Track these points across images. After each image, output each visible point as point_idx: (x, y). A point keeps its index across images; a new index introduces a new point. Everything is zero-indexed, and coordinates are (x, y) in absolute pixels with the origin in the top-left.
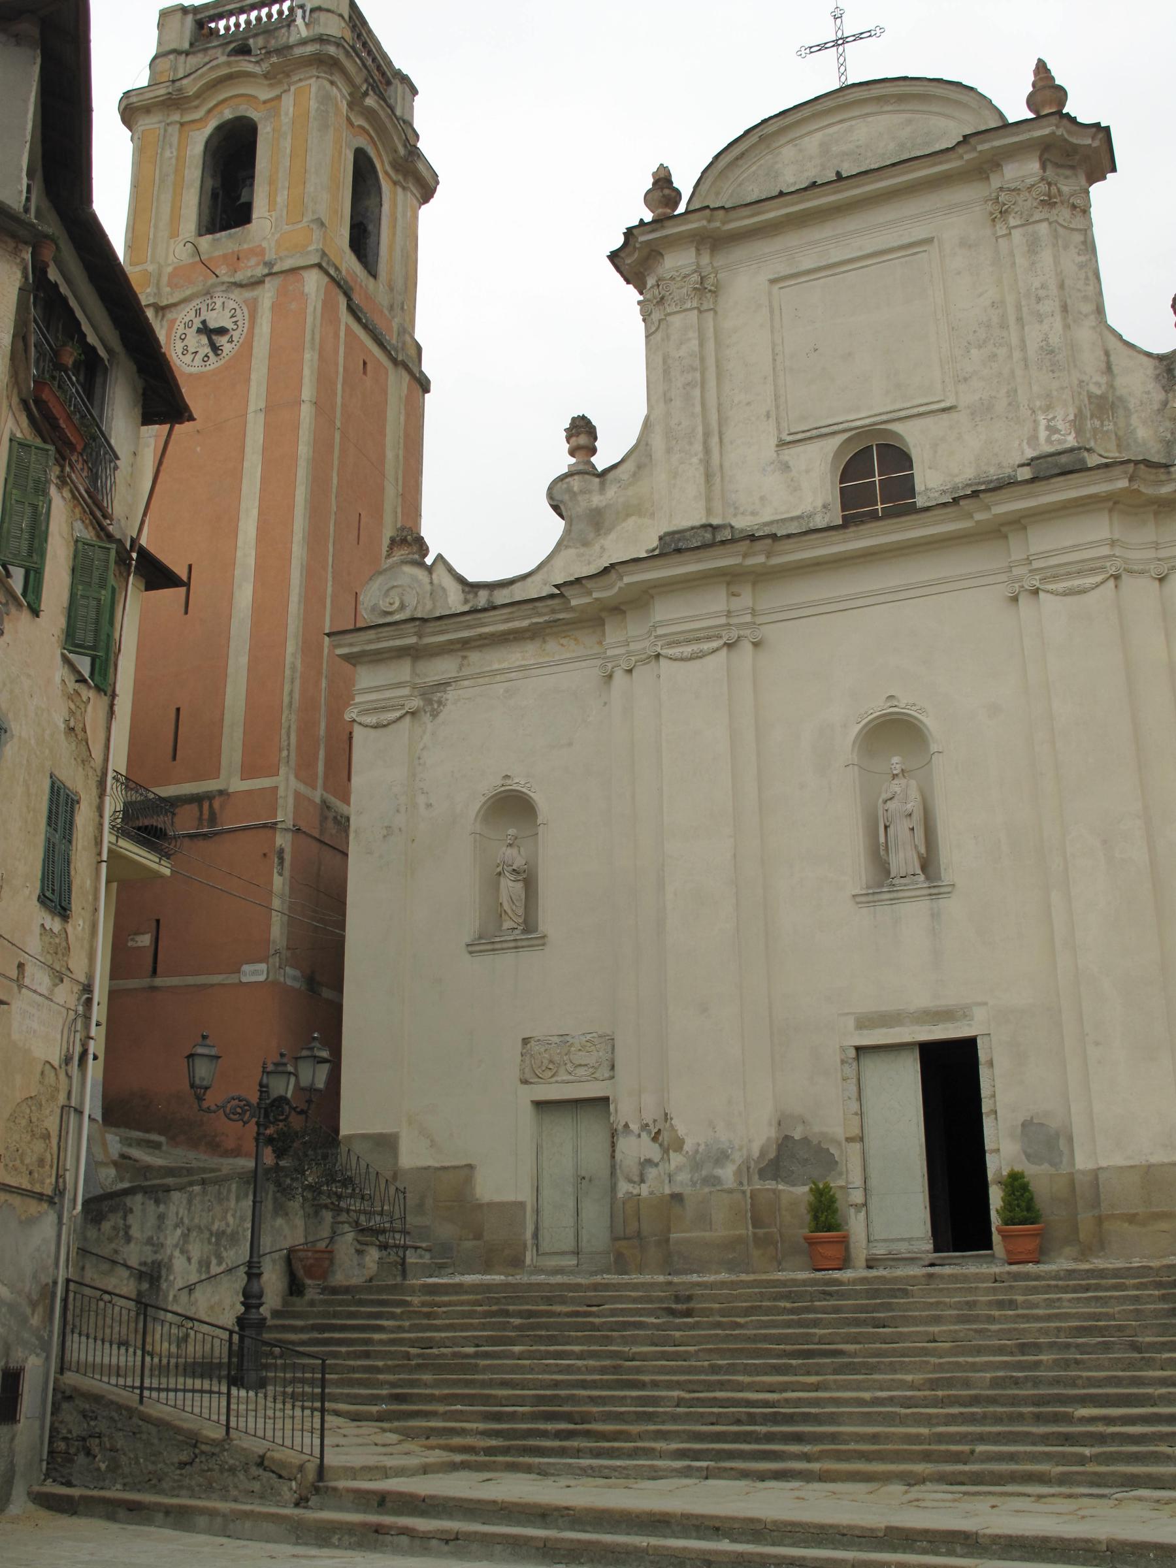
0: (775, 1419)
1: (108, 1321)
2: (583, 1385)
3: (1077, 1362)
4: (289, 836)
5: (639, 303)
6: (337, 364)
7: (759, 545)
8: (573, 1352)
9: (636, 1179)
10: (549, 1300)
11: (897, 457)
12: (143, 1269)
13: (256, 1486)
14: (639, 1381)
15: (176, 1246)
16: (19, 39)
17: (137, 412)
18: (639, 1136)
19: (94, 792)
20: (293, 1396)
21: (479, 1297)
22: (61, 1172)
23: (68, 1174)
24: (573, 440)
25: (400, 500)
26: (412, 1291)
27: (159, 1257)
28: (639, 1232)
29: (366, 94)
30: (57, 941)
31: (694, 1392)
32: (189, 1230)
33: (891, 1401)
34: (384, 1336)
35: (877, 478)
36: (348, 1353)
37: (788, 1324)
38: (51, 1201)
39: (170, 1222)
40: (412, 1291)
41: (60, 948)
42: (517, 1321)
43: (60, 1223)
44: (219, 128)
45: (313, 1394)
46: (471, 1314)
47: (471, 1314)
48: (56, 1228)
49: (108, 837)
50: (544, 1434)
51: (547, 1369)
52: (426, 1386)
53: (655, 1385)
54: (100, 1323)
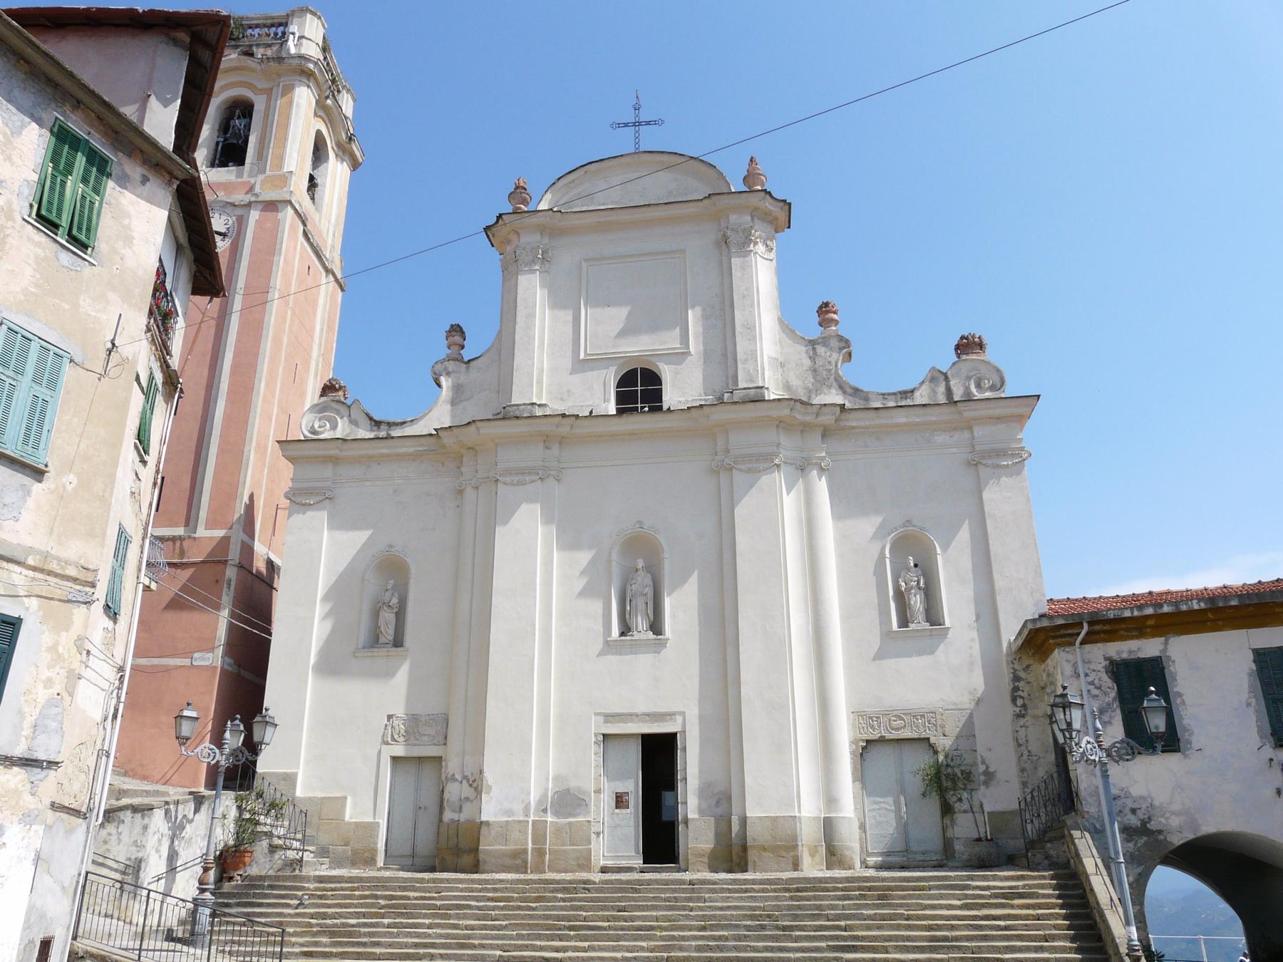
1: (98, 900)
2: (433, 946)
3: (746, 936)
4: (235, 569)
7: (566, 421)
16: (176, 42)
17: (189, 287)
20: (230, 953)
24: (451, 339)
27: (140, 855)
29: (327, 97)
37: (562, 909)
39: (151, 831)
40: (307, 879)
41: (110, 641)
42: (382, 902)
43: (88, 832)
44: (227, 100)
45: (274, 953)
46: (350, 897)
47: (350, 897)
51: (409, 935)
52: (325, 946)
53: (483, 946)
54: (92, 901)
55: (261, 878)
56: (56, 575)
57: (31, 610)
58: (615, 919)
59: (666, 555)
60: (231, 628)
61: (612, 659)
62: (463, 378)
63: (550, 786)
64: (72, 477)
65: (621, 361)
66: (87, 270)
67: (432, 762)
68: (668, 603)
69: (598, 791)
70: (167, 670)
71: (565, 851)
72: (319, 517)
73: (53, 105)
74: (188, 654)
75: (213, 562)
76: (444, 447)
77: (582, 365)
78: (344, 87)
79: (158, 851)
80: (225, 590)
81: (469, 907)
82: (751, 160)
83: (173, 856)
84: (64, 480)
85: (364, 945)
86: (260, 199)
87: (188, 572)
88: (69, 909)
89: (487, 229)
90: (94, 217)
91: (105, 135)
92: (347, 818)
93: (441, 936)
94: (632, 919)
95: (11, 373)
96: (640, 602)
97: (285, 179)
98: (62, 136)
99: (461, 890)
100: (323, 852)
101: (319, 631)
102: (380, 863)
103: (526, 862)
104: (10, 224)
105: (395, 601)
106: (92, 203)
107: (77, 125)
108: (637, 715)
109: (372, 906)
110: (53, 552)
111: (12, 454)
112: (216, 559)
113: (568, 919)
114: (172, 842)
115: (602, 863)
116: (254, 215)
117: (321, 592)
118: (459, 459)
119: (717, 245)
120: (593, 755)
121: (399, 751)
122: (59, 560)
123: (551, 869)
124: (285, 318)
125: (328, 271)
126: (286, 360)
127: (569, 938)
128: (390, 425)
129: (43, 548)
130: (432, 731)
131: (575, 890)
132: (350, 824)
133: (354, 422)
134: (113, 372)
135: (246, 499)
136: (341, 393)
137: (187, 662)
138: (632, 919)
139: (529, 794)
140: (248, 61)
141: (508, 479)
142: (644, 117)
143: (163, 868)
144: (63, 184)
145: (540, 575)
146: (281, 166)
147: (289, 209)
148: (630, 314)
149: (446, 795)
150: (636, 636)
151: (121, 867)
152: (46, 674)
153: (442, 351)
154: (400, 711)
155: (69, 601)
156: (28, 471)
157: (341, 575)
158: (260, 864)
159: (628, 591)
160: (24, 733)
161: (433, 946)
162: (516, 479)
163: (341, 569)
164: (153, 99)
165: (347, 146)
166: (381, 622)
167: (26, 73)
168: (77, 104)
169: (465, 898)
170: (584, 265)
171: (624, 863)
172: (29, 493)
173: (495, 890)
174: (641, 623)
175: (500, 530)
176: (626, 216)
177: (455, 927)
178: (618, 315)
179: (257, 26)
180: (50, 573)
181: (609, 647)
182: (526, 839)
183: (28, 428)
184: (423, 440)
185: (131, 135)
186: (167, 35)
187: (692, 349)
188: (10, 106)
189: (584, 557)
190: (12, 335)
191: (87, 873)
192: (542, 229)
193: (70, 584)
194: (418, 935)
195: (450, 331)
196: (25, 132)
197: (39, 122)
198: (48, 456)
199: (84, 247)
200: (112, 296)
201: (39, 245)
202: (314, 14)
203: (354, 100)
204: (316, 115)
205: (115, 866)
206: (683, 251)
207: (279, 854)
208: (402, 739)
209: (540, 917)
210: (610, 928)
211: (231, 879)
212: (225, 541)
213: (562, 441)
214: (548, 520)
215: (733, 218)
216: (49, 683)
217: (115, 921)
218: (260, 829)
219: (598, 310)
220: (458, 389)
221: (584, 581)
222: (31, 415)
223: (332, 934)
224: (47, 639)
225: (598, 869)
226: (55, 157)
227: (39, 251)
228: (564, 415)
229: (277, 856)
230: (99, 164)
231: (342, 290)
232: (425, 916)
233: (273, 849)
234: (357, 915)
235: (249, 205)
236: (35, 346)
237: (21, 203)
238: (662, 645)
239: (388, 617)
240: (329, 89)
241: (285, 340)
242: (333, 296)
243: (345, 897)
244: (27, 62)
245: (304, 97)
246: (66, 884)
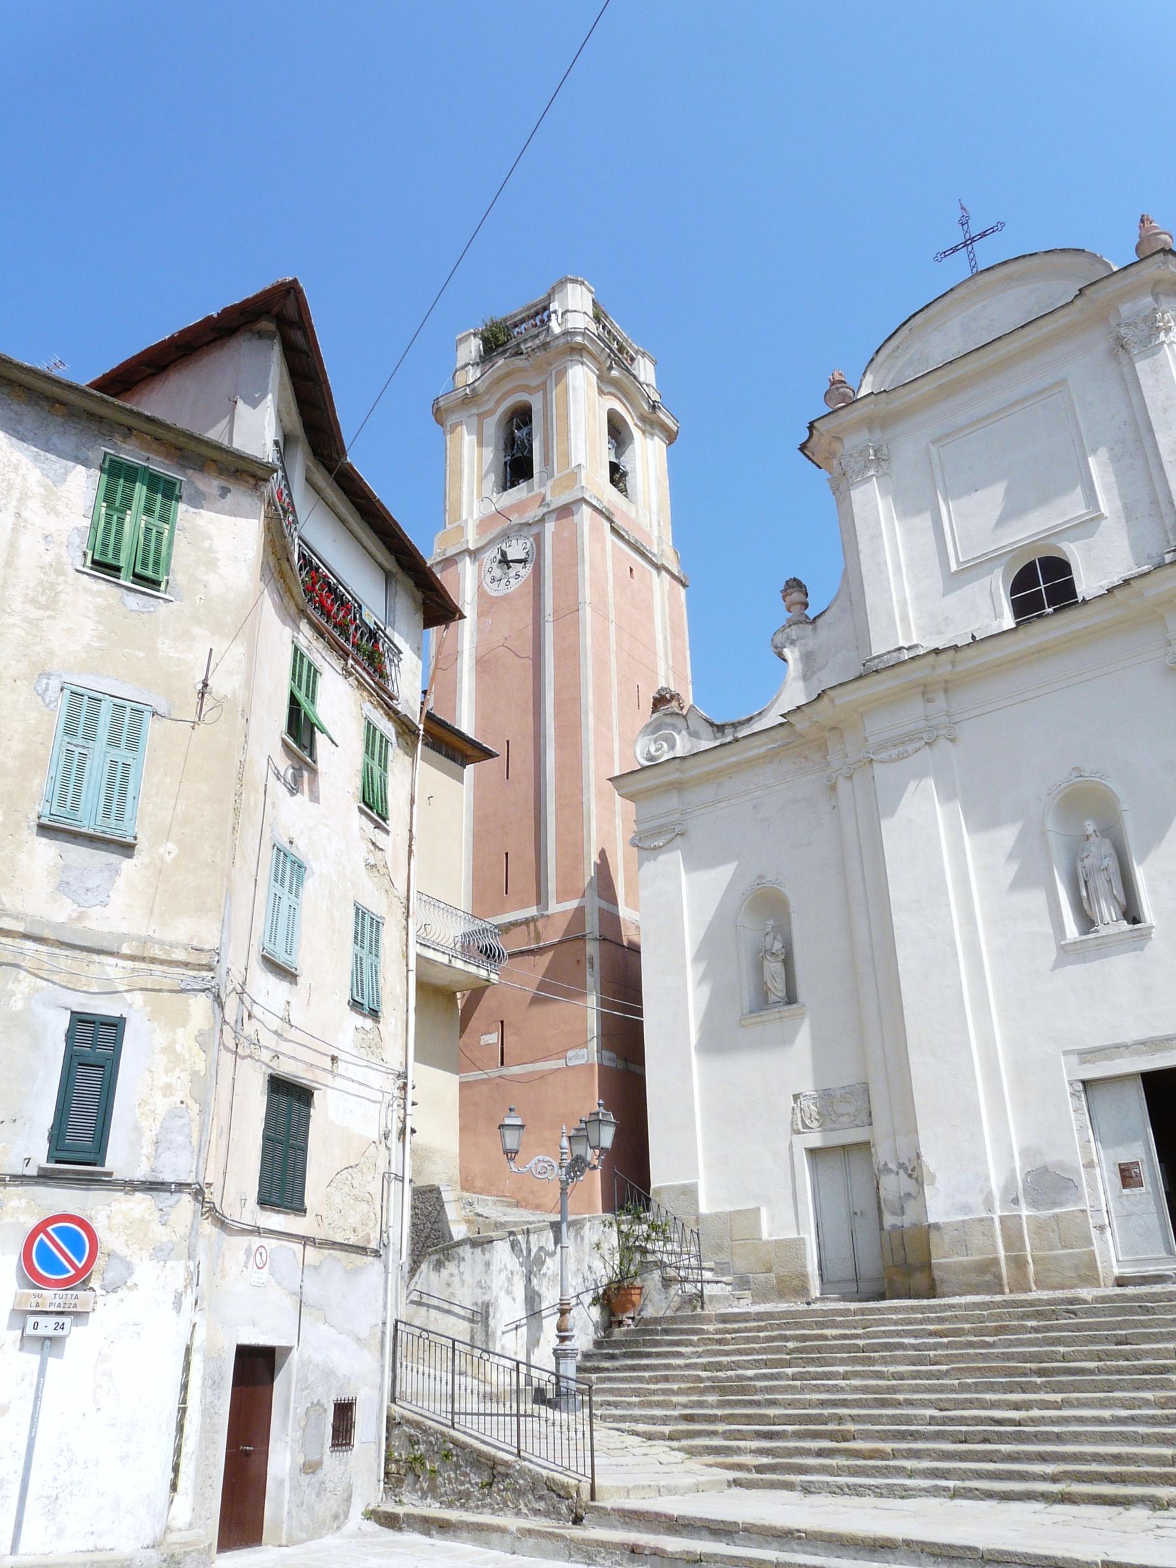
0: (1020, 1438)
2: (844, 1403)
5: (828, 480)
6: (606, 572)
7: (943, 657)
8: (838, 1373)
9: (899, 1211)
10: (822, 1325)
11: (1057, 568)
12: (475, 1308)
13: (541, 1505)
14: (896, 1400)
15: (501, 1288)
16: (261, 335)
17: (419, 618)
18: (898, 1173)
19: (400, 916)
21: (763, 1324)
22: (384, 1229)
23: (391, 1230)
24: (788, 598)
25: (671, 672)
26: (707, 1319)
27: (486, 1298)
28: (905, 1260)
29: (610, 368)
30: (370, 1036)
31: (946, 1410)
32: (512, 1273)
33: (1133, 1420)
34: (681, 1362)
35: (1042, 587)
36: (650, 1377)
37: (1032, 1343)
38: (377, 1254)
39: (494, 1268)
40: (707, 1319)
44: (505, 414)
47: (755, 1340)
48: (384, 1276)
49: (414, 949)
50: (807, 1452)
52: (712, 1407)
53: (910, 1403)
55: (656, 1321)
56: (162, 962)
57: (135, 1007)
58: (1110, 1355)
59: (1124, 807)
60: (604, 1018)
61: (1074, 970)
62: (811, 643)
63: (1018, 1165)
64: (171, 846)
65: (1009, 557)
66: (163, 608)
67: (856, 1150)
68: (1140, 874)
69: (1089, 1165)
70: (542, 1076)
71: (1055, 1258)
72: (674, 859)
73: (100, 441)
74: (561, 1054)
75: (571, 940)
76: (801, 736)
77: (955, 579)
78: (637, 352)
79: (508, 1292)
80: (588, 971)
81: (901, 1346)
82: (1142, 221)
83: (532, 1299)
84: (161, 850)
85: (757, 1404)
86: (553, 507)
87: (545, 960)
88: (376, 1365)
89: (802, 448)
90: (164, 549)
91: (168, 456)
92: (765, 1236)
93: (856, 1389)
94: (1137, 1355)
95: (80, 741)
96: (1100, 882)
97: (573, 476)
98: (116, 471)
99: (896, 1323)
100: (742, 1283)
101: (695, 1000)
102: (815, 1292)
103: (999, 1277)
104: (61, 578)
105: (778, 946)
106: (160, 533)
107: (130, 454)
108: (1127, 1047)
109: (778, 1350)
110: (156, 936)
111: (91, 832)
112: (574, 938)
113: (1038, 1358)
114: (529, 1280)
115: (1117, 1271)
116: (550, 527)
117: (689, 951)
118: (822, 746)
119: (1112, 355)
120: (1074, 1112)
121: (815, 1140)
122: (161, 943)
123: (1041, 1285)
124: (606, 637)
125: (659, 568)
126: (619, 682)
127: (1036, 1388)
128: (735, 726)
129: (143, 933)
130: (851, 1109)
131: (1054, 1314)
132: (768, 1242)
133: (694, 734)
134: (208, 718)
135: (595, 858)
136: (674, 703)
137: (561, 1063)
138: (1137, 1355)
139: (987, 1179)
140: (519, 362)
141: (884, 755)
142: (975, 231)
143: (520, 1312)
144: (121, 521)
145: (952, 874)
146: (569, 463)
147: (584, 507)
148: (1008, 490)
149: (882, 1193)
150: (1103, 930)
151: (469, 1314)
152: (163, 1079)
153: (781, 614)
154: (807, 1088)
155: (182, 991)
156: (112, 847)
157: (711, 925)
158: (656, 1303)
159: (1080, 869)
160: (144, 1151)
161: (844, 1403)
162: (894, 752)
163: (709, 918)
164: (240, 403)
165: (652, 417)
166: (768, 980)
167: (64, 416)
168: (129, 432)
169: (898, 1334)
170: (933, 448)
171: (1151, 1270)
172: (117, 872)
173: (941, 1320)
174: (1107, 911)
175: (885, 824)
176: (972, 364)
177: (879, 1375)
178: (993, 497)
179: (522, 321)
180: (153, 960)
181: (1067, 954)
182: (994, 1245)
183: (109, 799)
184: (772, 733)
185: (192, 445)
186: (251, 331)
187: (1104, 509)
188: (49, 455)
189: (1008, 835)
190: (77, 699)
191: (397, 1322)
192: (869, 423)
193: (180, 971)
194: (828, 1390)
195: (785, 590)
196: (70, 478)
197: (86, 463)
198: (140, 825)
199: (154, 583)
200: (196, 630)
201: (99, 594)
202: (575, 281)
203: (655, 363)
204: (601, 392)
205: (462, 1312)
206: (1064, 381)
207: (675, 1289)
208: (815, 1124)
209: (997, 1357)
210: (1100, 1371)
211: (620, 1323)
212: (580, 910)
213: (947, 687)
214: (947, 796)
215: (1126, 309)
216: (168, 1090)
217: (469, 1379)
218: (650, 1258)
219: (964, 500)
220: (808, 659)
221: (1014, 867)
222: (111, 784)
223: (723, 1390)
224: (160, 1038)
225: (1111, 1281)
226: (109, 498)
227: (100, 601)
228: (937, 651)
229: (672, 1292)
230: (167, 490)
231: (685, 586)
232: (842, 1362)
233: (667, 1282)
234: (758, 1364)
235: (542, 520)
236: (106, 708)
237: (74, 558)
238: (1146, 936)
239: (774, 968)
240: (614, 362)
241: (613, 660)
242: (672, 597)
243: (748, 1340)
244: (62, 403)
245: (581, 378)
246: (364, 1334)
